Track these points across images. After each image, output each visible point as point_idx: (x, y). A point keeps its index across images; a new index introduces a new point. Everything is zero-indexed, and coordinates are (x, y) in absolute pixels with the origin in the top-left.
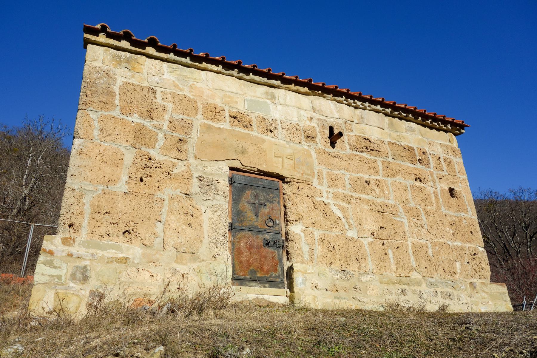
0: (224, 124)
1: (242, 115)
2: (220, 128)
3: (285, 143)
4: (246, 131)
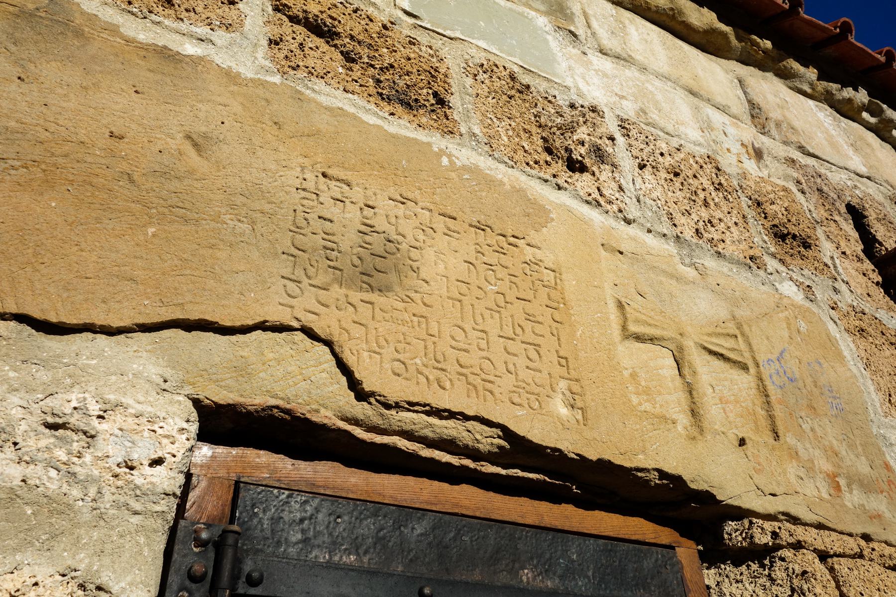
0: (221, 37)
1: (375, 28)
2: (166, 54)
3: (671, 248)
4: (402, 126)
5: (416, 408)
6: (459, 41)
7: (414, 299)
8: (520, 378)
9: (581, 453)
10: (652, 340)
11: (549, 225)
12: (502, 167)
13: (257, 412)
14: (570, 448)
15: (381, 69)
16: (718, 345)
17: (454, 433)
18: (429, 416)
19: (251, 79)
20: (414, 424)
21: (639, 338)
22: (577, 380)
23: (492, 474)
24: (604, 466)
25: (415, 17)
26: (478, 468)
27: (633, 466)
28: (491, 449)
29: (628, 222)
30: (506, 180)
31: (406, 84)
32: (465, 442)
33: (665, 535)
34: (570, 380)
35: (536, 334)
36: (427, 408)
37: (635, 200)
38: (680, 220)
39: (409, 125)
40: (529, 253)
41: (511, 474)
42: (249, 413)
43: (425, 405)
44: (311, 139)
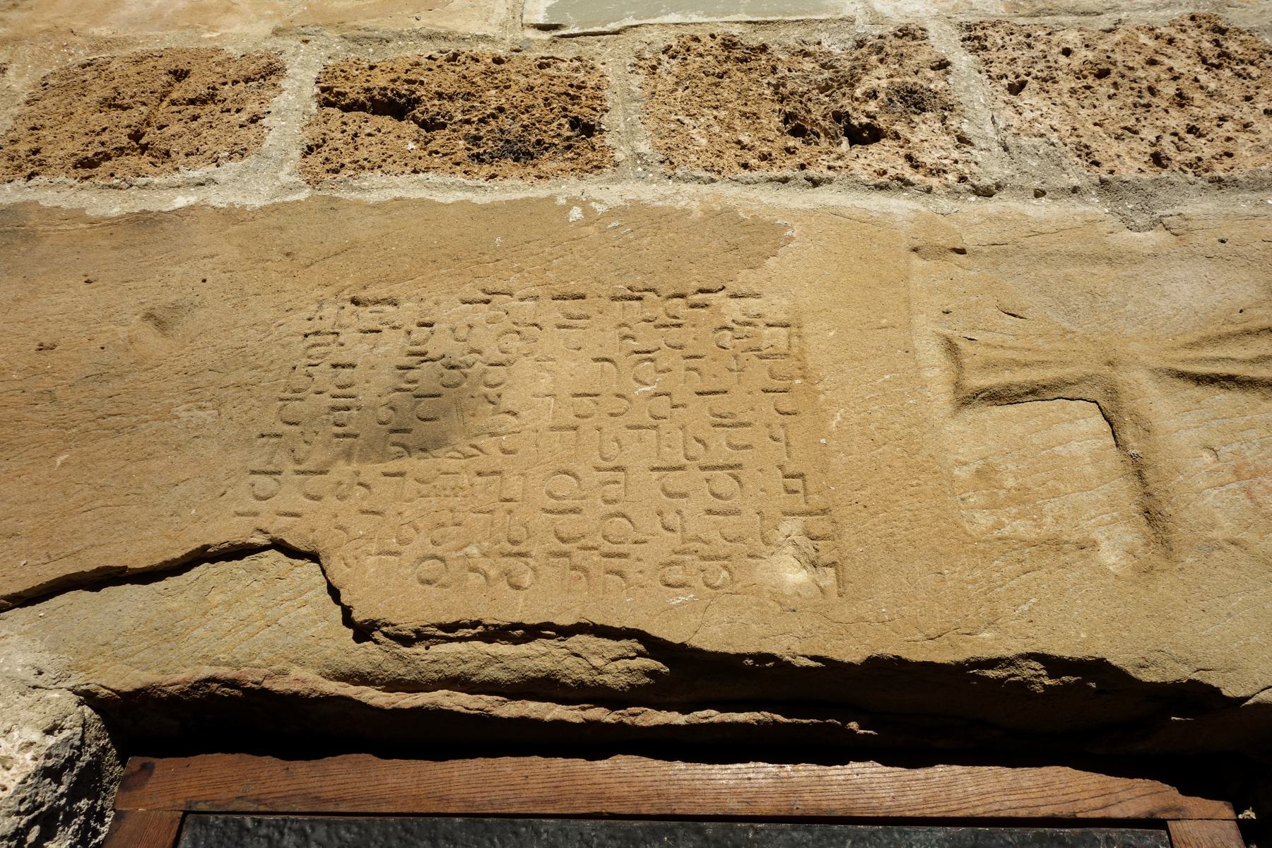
2: (144, 221)
3: (1095, 207)
4: (514, 187)
5: (460, 633)
6: (630, 31)
7: (484, 447)
8: (691, 534)
9: (822, 653)
10: (1034, 392)
11: (781, 251)
12: (690, 188)
13: (186, 693)
14: (797, 648)
15: (481, 121)
16: (1218, 360)
17: (547, 664)
18: (490, 642)
19: (261, 209)
20: (465, 662)
21: (996, 397)
22: (824, 512)
23: (657, 727)
24: (883, 669)
25: (556, 27)
26: (627, 720)
27: (960, 657)
28: (632, 680)
29: (986, 193)
30: (695, 205)
31: (523, 126)
32: (575, 677)
33: (1133, 796)
34: (809, 513)
35: (736, 447)
36: (480, 629)
37: (997, 150)
38: (1106, 148)
39: (520, 182)
40: (733, 310)
41: (694, 721)
42: (172, 697)
43: (474, 624)
44: (340, 258)
